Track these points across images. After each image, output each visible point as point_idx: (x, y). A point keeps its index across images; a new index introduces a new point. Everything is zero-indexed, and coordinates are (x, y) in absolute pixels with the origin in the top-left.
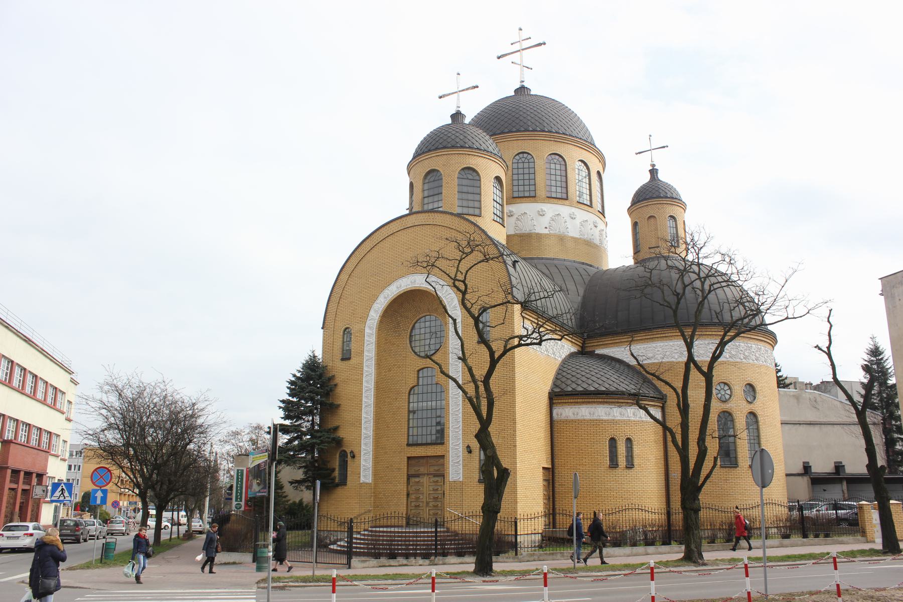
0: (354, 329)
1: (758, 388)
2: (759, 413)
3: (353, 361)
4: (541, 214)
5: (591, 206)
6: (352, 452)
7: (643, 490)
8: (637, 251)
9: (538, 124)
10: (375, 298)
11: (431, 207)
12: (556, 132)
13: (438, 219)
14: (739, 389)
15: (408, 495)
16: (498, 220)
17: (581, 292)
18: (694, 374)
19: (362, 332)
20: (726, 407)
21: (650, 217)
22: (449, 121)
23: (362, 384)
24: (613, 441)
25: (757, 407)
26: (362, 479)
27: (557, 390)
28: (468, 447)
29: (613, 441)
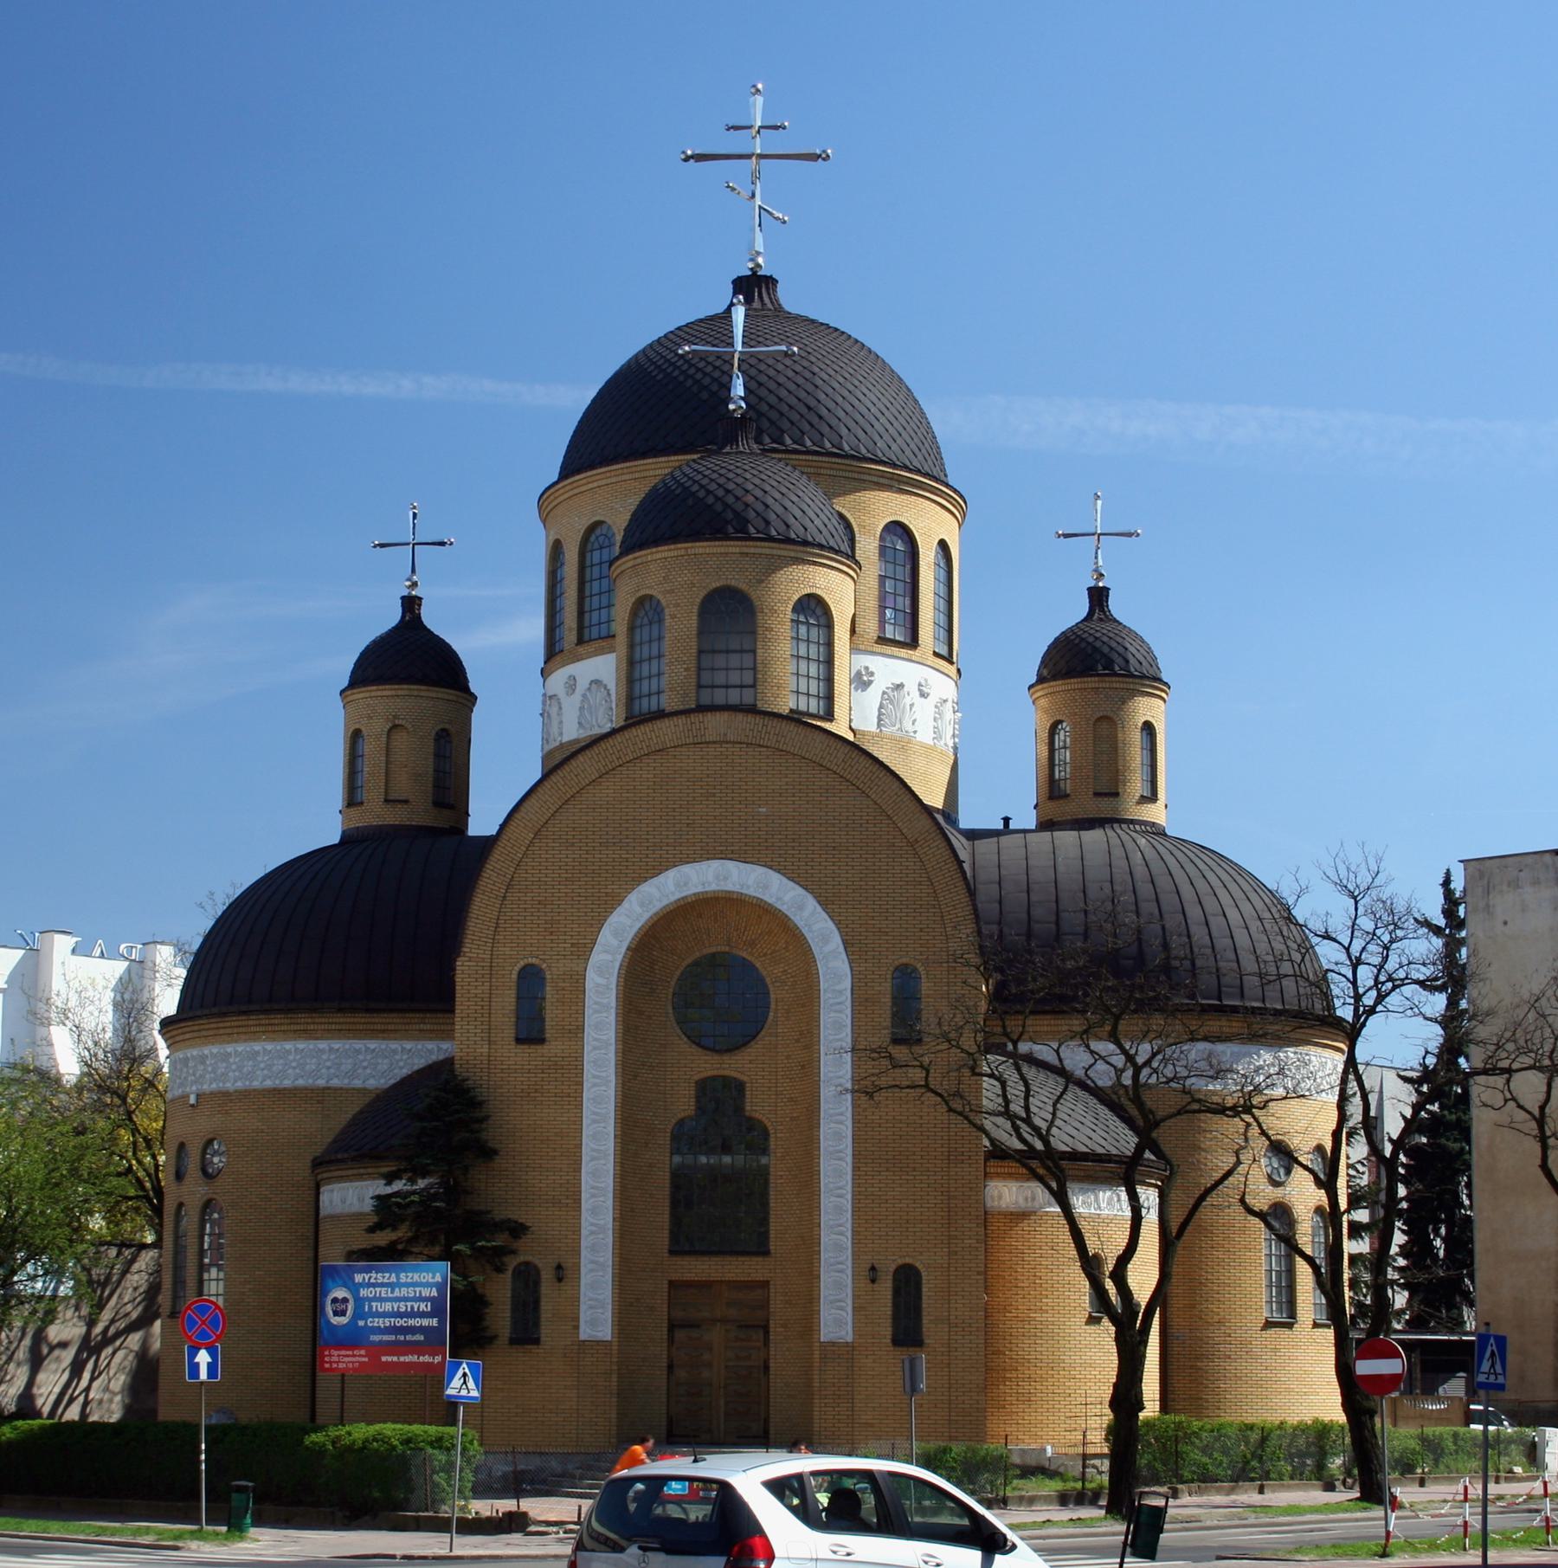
0: (554, 971)
3: (554, 1047)
8: (352, 800)
10: (614, 901)
13: (715, 724)
15: (670, 1367)
19: (578, 981)
26: (585, 1333)
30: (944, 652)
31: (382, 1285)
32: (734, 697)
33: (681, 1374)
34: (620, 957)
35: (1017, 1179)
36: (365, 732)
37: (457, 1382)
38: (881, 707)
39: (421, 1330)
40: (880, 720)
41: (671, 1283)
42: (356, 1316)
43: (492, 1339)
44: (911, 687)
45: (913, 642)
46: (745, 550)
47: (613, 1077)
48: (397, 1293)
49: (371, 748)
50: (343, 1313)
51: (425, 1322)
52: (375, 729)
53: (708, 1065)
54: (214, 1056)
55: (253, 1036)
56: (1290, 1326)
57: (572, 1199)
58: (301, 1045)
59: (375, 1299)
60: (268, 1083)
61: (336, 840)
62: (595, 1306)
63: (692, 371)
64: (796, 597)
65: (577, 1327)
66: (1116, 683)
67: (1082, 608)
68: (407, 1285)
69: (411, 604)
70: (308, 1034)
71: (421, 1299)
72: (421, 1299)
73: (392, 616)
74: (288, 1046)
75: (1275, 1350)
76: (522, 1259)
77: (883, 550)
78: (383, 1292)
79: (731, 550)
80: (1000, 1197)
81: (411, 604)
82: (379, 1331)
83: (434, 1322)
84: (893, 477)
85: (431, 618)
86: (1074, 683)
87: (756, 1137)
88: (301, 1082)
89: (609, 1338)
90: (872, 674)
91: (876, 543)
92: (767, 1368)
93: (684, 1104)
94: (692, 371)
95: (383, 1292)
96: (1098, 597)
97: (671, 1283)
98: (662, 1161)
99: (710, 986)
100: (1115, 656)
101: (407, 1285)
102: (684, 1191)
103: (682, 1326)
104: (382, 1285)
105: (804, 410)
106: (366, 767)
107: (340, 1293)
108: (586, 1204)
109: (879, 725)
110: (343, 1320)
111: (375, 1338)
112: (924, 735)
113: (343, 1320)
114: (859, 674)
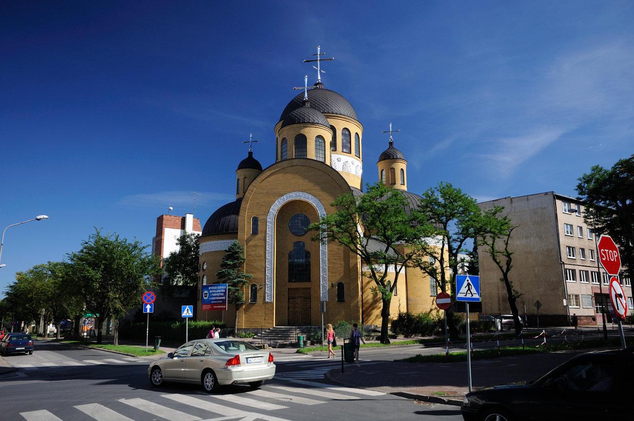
0: (260, 218)
15: (289, 308)
21: (338, 161)
30: (358, 156)
31: (214, 290)
32: (303, 157)
33: (291, 309)
36: (240, 179)
37: (185, 312)
39: (220, 300)
41: (289, 288)
42: (209, 297)
44: (350, 162)
45: (350, 153)
48: (217, 291)
49: (241, 182)
50: (206, 297)
51: (222, 298)
52: (241, 178)
53: (296, 239)
54: (209, 244)
55: (211, 240)
58: (221, 241)
59: (213, 293)
60: (214, 250)
61: (235, 201)
62: (270, 293)
68: (219, 289)
69: (250, 154)
70: (222, 239)
71: (222, 293)
72: (222, 293)
73: (246, 156)
74: (218, 242)
77: (343, 134)
78: (214, 291)
81: (250, 154)
82: (213, 300)
83: (224, 298)
84: (332, 116)
85: (255, 156)
86: (386, 161)
87: (307, 255)
88: (221, 249)
92: (310, 308)
93: (291, 248)
95: (214, 291)
96: (391, 144)
97: (289, 288)
98: (286, 261)
99: (294, 218)
100: (391, 155)
101: (219, 289)
102: (291, 266)
103: (291, 298)
104: (214, 290)
106: (240, 186)
107: (206, 292)
110: (206, 298)
111: (212, 302)
112: (353, 172)
113: (206, 298)
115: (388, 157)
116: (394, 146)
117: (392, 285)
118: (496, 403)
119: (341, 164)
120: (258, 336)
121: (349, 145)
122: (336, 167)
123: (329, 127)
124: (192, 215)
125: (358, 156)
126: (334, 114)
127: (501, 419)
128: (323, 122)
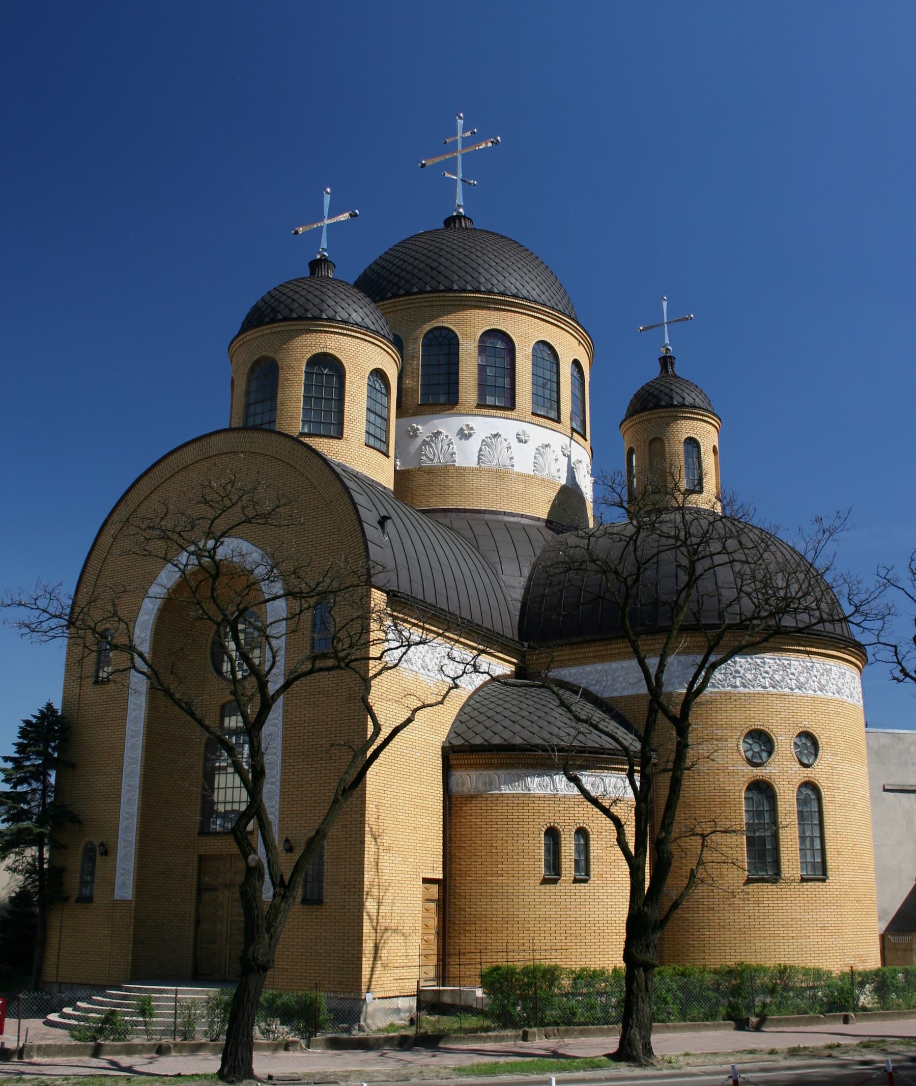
1: (822, 741)
2: (823, 783)
4: (464, 435)
5: (558, 421)
6: (102, 844)
7: (586, 925)
9: (469, 278)
11: (258, 421)
12: (502, 294)
14: (785, 742)
16: (378, 444)
17: (526, 572)
18: (662, 720)
20: (759, 773)
21: (520, 441)
22: (306, 272)
23: (124, 727)
24: (553, 834)
25: (819, 773)
27: (458, 742)
28: (287, 841)
29: (553, 834)
30: (385, 415)
34: (153, 616)
35: (476, 769)
38: (481, 450)
40: (479, 459)
43: (66, 899)
46: (273, 330)
47: (144, 704)
56: (824, 880)
57: (116, 798)
63: (396, 280)
64: (308, 356)
65: (113, 890)
66: (662, 413)
67: (655, 371)
75: (758, 902)
76: (88, 839)
79: (265, 332)
80: (463, 784)
84: (489, 301)
89: (130, 898)
90: (472, 429)
91: (476, 344)
94: (403, 282)
96: (666, 362)
100: (662, 396)
105: (428, 270)
108: (123, 799)
109: (479, 463)
114: (462, 430)
115: (656, 403)
116: (679, 369)
117: (620, 748)
118: (647, 883)
119: (529, 450)
120: (77, 1009)
121: (507, 381)
122: (456, 457)
123: (389, 340)
124: (879, 965)
125: (553, 414)
126: (495, 294)
127: (3, 770)
128: (367, 320)
